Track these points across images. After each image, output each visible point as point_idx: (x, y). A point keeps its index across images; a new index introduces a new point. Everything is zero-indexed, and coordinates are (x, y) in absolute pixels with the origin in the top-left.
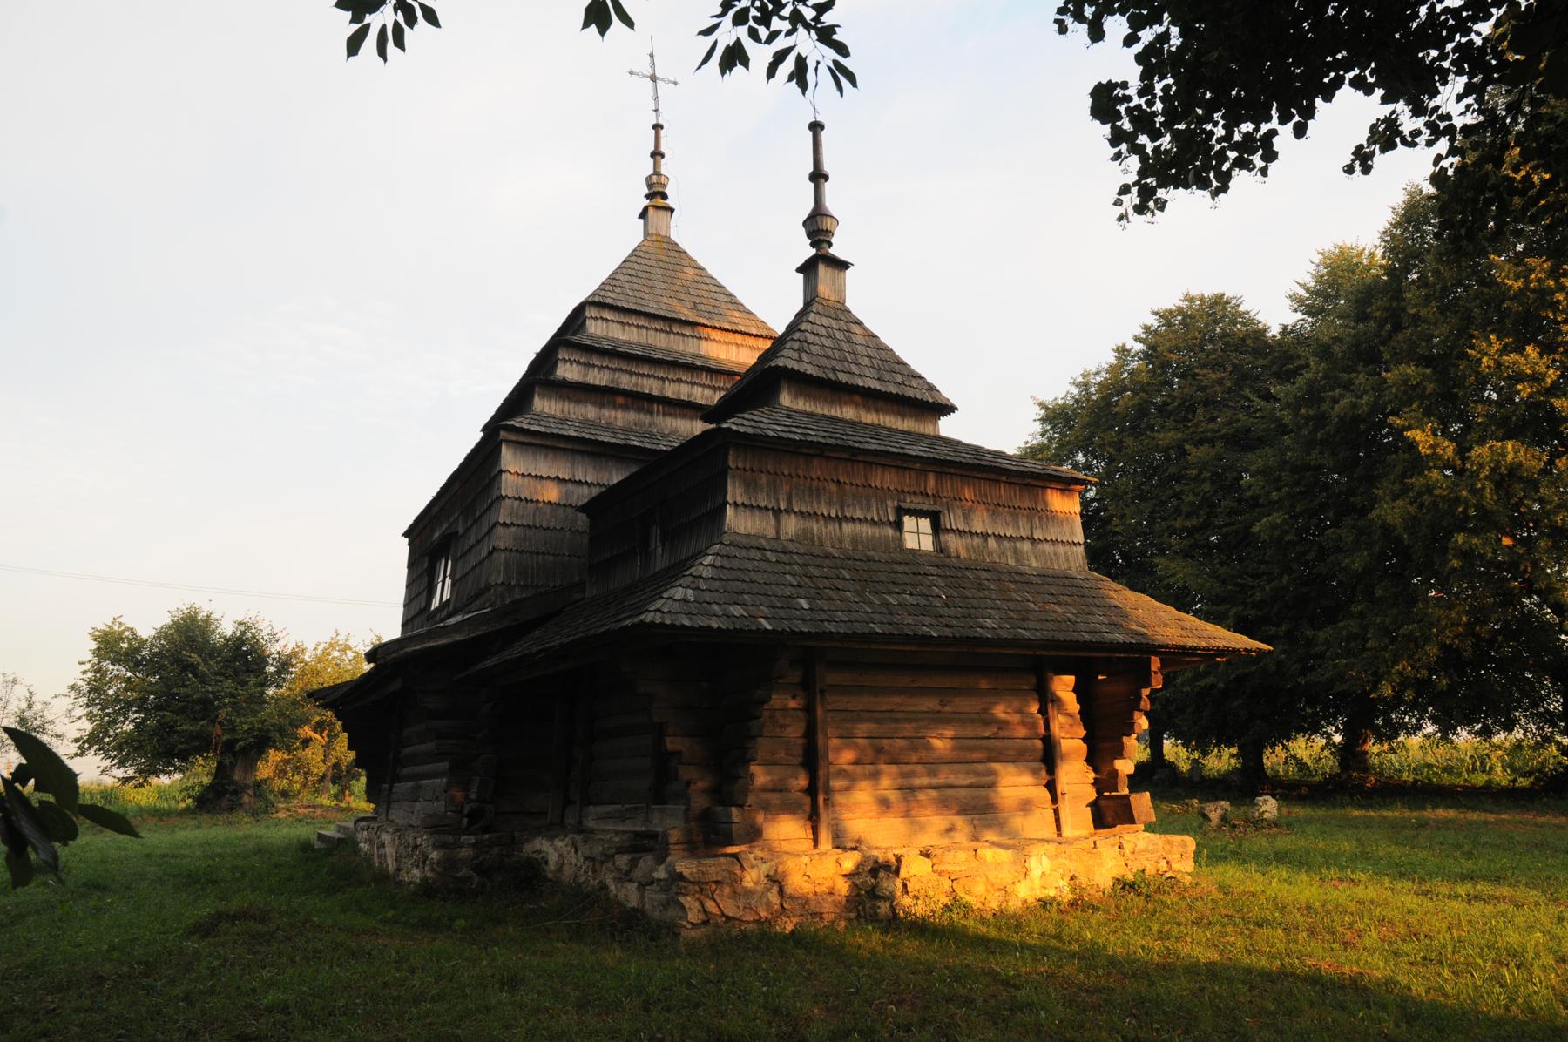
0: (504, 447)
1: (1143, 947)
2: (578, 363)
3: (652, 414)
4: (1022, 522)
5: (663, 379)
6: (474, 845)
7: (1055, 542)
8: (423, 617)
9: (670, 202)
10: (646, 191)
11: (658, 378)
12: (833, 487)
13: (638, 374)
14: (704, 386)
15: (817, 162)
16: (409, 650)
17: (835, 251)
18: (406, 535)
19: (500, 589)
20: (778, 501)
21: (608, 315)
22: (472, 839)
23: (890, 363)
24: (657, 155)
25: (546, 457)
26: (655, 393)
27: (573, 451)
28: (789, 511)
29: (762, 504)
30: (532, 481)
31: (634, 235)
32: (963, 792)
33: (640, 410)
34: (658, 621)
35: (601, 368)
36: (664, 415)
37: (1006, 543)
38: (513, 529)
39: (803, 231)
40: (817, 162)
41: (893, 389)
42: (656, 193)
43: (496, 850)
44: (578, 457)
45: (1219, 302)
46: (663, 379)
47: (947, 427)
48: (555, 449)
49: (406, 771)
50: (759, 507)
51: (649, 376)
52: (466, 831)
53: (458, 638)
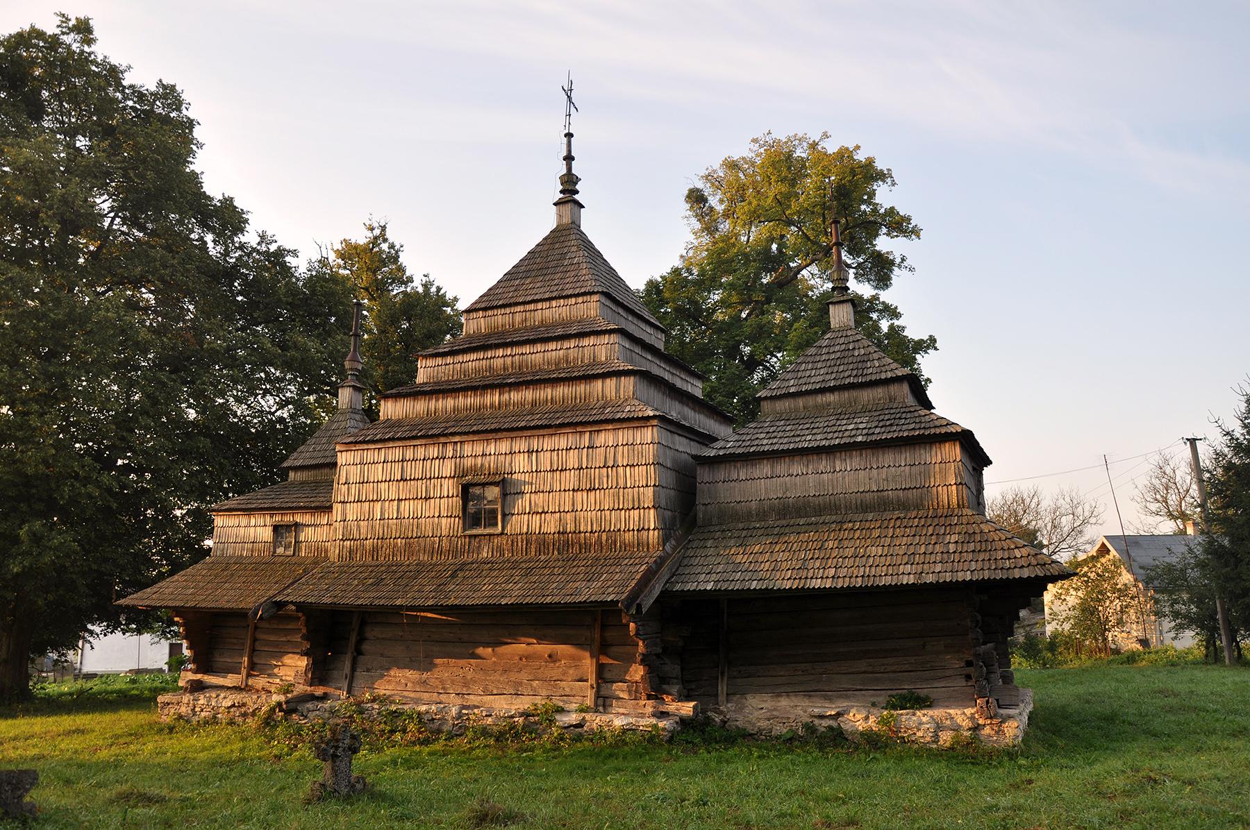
24: (569, 158)
42: (570, 183)
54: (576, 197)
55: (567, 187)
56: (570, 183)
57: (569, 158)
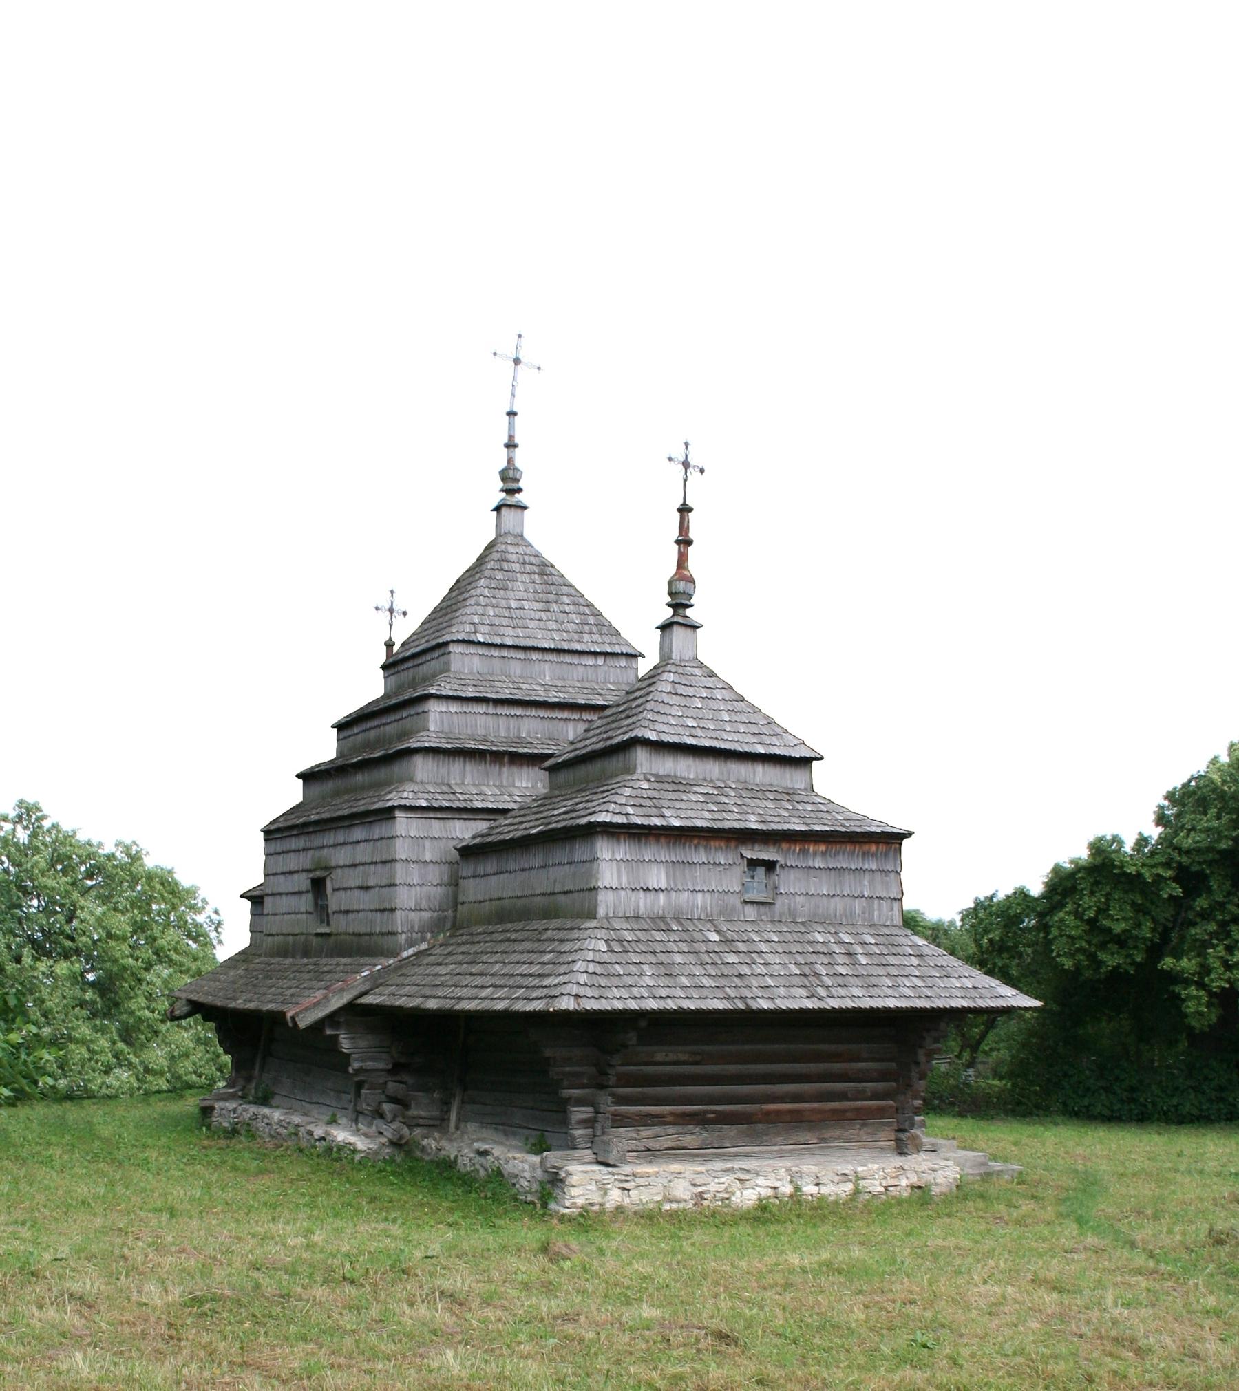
24: (511, 445)
42: (510, 480)
54: (518, 497)
55: (511, 500)
56: (510, 480)
57: (511, 445)
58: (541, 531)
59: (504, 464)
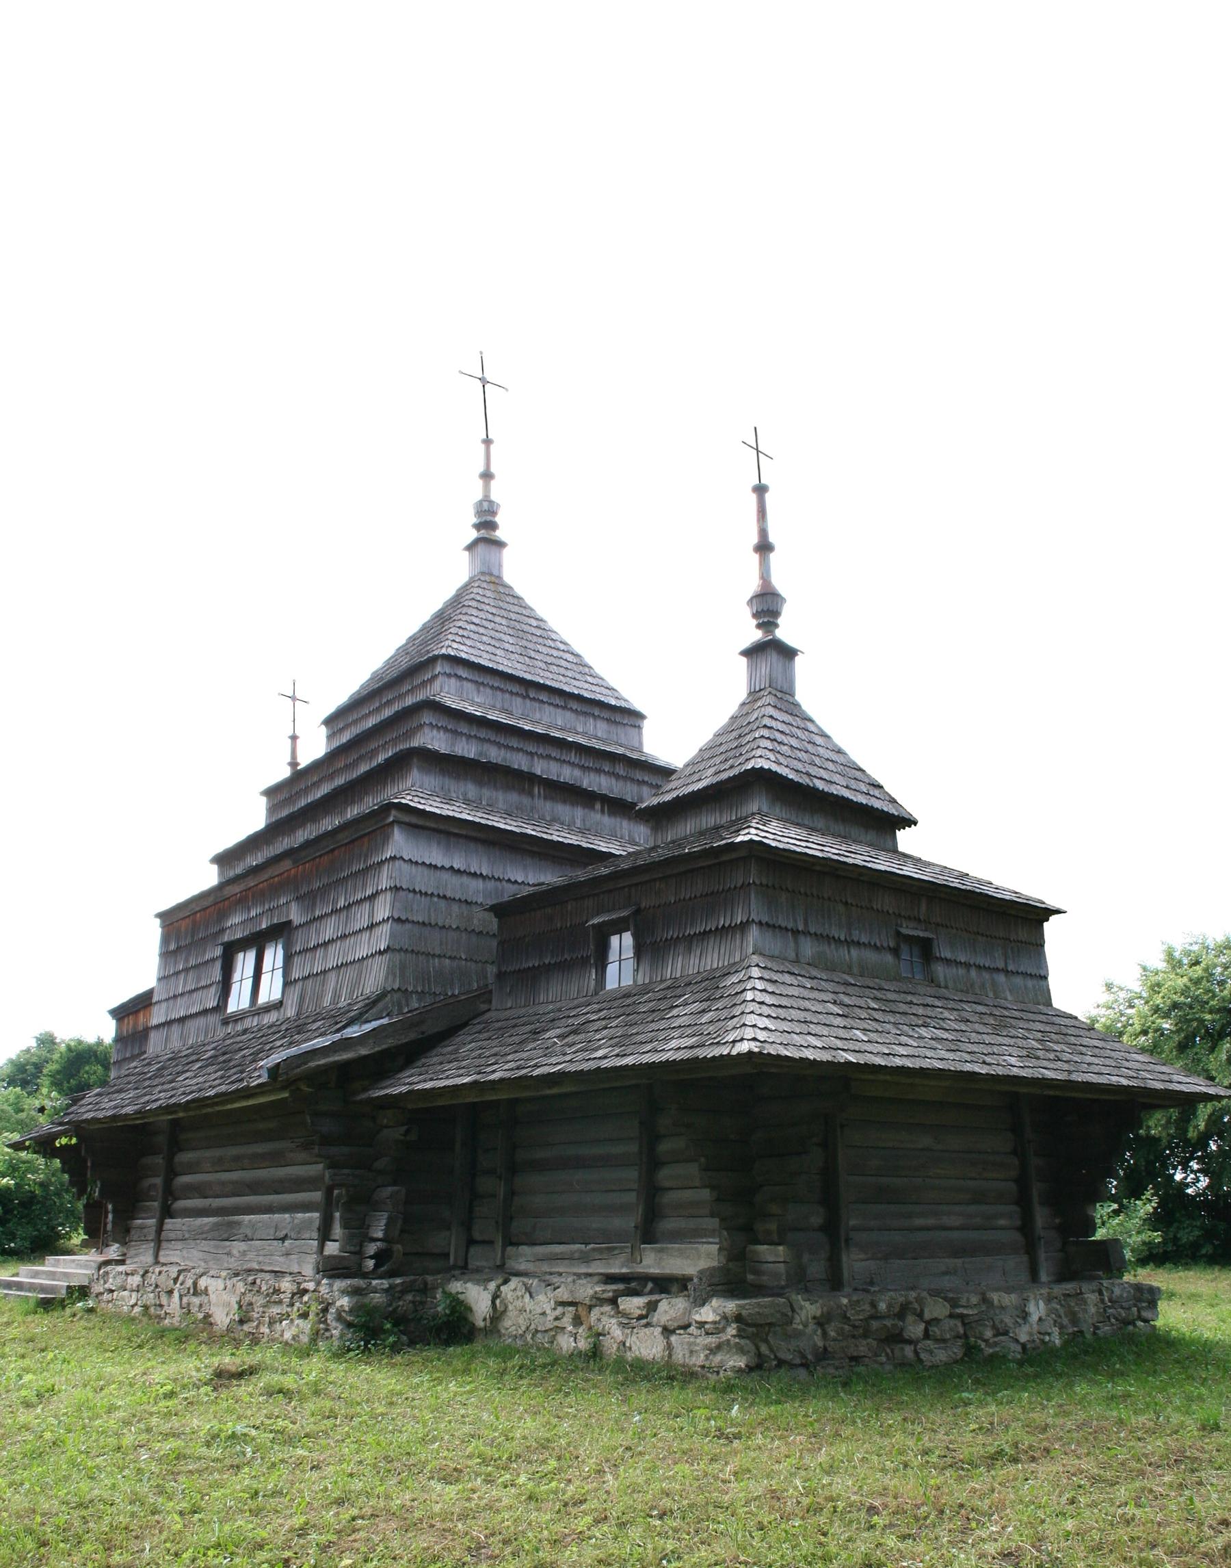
0: (396, 831)
1: (1200, 1398)
2: (446, 729)
3: (533, 797)
4: (998, 954)
5: (531, 754)
6: (386, 1291)
7: (1025, 975)
8: (213, 1019)
9: (500, 534)
10: (475, 520)
11: (527, 753)
12: (841, 908)
13: (507, 747)
14: (572, 764)
15: (763, 533)
16: (312, 1064)
17: (782, 634)
18: (162, 916)
19: (396, 996)
20: (795, 921)
21: (462, 672)
22: (385, 1283)
23: (854, 763)
24: (487, 476)
25: (439, 843)
26: (525, 768)
27: (467, 837)
28: (806, 933)
29: (783, 925)
30: (426, 871)
31: (457, 570)
32: (955, 1235)
33: (522, 791)
34: (756, 1050)
35: (469, 737)
36: (545, 798)
37: (986, 975)
38: (408, 926)
39: (747, 612)
40: (763, 533)
41: (539, 730)
42: (486, 522)
43: (409, 1297)
44: (472, 845)
45: (783, 600)
46: (531, 754)
47: (906, 840)
48: (449, 834)
49: (181, 1204)
50: (780, 927)
51: (518, 750)
52: (374, 1274)
53: (364, 1051)
55: (489, 518)
56: (486, 522)
57: (487, 476)
58: (516, 570)
59: (479, 496)
